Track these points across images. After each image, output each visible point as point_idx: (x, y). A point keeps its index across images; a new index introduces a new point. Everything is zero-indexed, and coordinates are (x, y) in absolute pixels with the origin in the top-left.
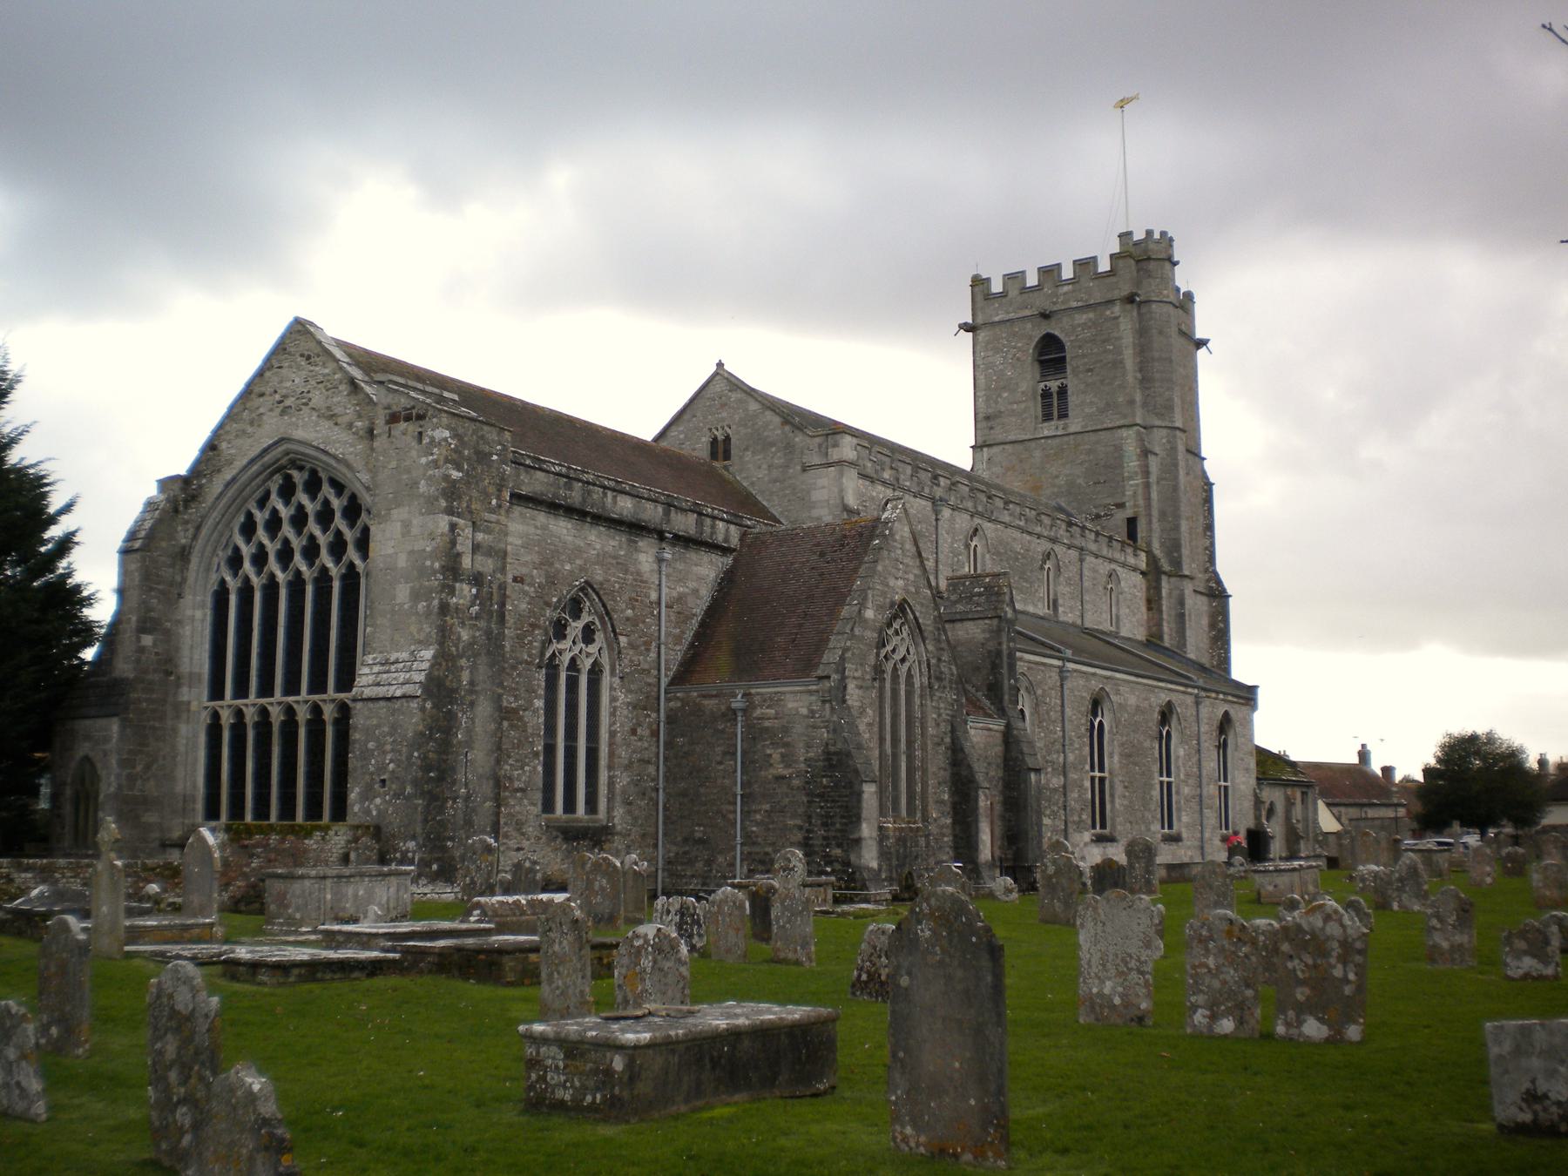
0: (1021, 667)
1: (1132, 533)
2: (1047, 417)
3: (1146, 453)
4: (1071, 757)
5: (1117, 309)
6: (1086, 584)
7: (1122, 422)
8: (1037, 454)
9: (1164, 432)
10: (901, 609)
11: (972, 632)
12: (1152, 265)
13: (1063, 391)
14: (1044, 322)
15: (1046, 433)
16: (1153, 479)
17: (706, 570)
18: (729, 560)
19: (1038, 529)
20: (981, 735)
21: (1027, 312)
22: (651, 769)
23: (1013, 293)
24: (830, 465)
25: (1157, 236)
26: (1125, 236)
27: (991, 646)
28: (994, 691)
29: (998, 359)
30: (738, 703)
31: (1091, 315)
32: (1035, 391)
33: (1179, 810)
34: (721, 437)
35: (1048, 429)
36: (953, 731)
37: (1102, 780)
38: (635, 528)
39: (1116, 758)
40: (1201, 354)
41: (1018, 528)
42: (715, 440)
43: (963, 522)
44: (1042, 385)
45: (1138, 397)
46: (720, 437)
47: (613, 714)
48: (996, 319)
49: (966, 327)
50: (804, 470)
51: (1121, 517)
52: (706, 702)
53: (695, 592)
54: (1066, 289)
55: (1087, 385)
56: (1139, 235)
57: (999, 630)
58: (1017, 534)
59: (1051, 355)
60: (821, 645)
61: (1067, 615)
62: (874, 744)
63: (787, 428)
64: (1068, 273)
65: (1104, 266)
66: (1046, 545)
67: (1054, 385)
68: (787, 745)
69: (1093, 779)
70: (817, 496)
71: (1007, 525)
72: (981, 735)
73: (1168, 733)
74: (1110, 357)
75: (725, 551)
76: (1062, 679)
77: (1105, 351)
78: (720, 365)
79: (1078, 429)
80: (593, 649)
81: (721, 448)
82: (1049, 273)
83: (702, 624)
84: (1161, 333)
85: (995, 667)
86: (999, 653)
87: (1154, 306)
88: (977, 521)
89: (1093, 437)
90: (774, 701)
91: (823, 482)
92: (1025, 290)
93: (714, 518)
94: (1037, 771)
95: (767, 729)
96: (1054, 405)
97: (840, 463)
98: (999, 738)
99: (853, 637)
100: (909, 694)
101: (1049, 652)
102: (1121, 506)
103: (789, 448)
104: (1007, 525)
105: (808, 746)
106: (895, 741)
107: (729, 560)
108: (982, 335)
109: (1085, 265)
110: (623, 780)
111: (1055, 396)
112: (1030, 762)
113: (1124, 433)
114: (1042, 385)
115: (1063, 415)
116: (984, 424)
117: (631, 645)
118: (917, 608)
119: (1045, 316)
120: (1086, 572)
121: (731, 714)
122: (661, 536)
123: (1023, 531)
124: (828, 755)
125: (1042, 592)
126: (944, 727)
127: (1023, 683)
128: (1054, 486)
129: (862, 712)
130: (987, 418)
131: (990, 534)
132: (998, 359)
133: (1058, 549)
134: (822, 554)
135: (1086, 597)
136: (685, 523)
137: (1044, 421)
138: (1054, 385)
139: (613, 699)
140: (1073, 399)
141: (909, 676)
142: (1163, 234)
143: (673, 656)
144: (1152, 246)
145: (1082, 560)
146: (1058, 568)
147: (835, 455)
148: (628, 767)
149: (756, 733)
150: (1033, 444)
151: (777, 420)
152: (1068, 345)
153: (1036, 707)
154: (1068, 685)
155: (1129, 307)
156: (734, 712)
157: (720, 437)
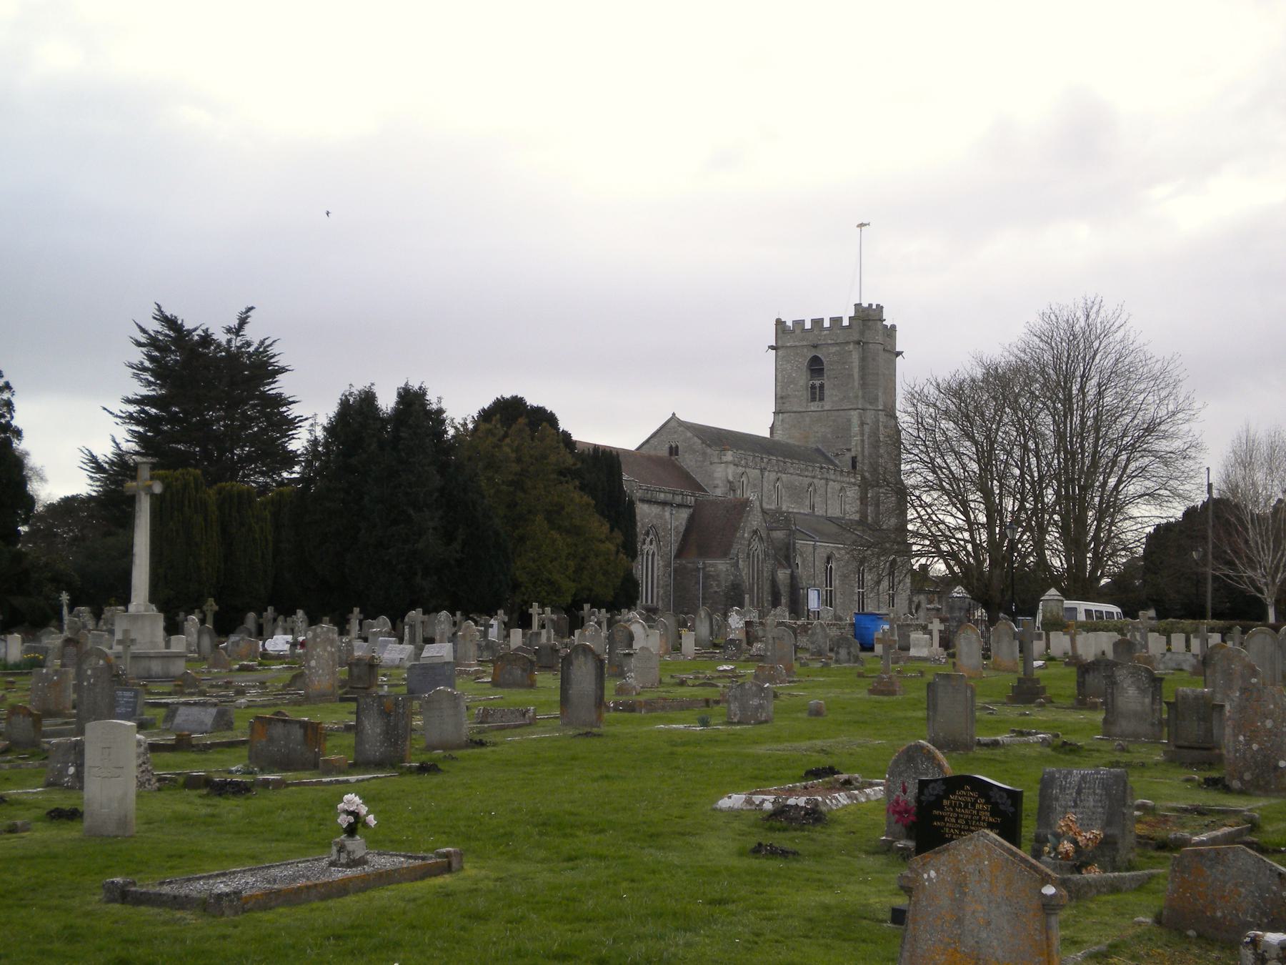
0: (798, 546)
1: (854, 466)
2: (813, 399)
3: (862, 424)
4: (817, 582)
5: (851, 346)
6: (829, 495)
7: (851, 407)
8: (808, 419)
9: (873, 412)
10: (755, 532)
11: (779, 535)
12: (870, 323)
13: (822, 386)
14: (813, 350)
15: (812, 409)
16: (866, 437)
17: (684, 514)
18: (692, 510)
19: (806, 473)
20: (783, 575)
21: (805, 343)
22: (669, 588)
23: (798, 331)
24: (722, 463)
25: (874, 307)
26: (858, 306)
27: (786, 541)
28: (787, 558)
29: (789, 367)
30: (701, 566)
31: (838, 348)
32: (807, 386)
33: (867, 604)
34: (674, 446)
35: (814, 406)
36: (773, 575)
37: (831, 591)
38: (664, 504)
39: (837, 582)
40: (899, 359)
41: (797, 474)
42: (671, 446)
43: (773, 476)
44: (811, 382)
45: (860, 394)
46: (154, 326)
47: (658, 569)
48: (788, 344)
49: (771, 347)
50: (711, 464)
51: (848, 456)
52: (689, 565)
53: (681, 523)
54: (825, 332)
55: (834, 385)
56: (865, 305)
57: (789, 535)
58: (797, 477)
59: (816, 367)
60: (730, 546)
61: (819, 511)
62: (747, 581)
63: (704, 445)
64: (827, 324)
65: (846, 323)
66: (809, 480)
67: (817, 383)
68: (718, 581)
69: (827, 591)
70: (716, 475)
71: (792, 474)
72: (783, 575)
73: (863, 570)
74: (847, 372)
75: (690, 507)
76: (815, 549)
77: (845, 369)
78: (674, 414)
79: (829, 408)
80: (652, 547)
81: (674, 451)
82: (817, 323)
83: (684, 535)
84: (874, 360)
85: (788, 549)
86: (789, 544)
87: (871, 345)
88: (779, 474)
89: (836, 413)
90: (713, 565)
91: (719, 469)
92: (804, 330)
93: (687, 495)
94: (803, 589)
95: (711, 575)
96: (816, 394)
97: (726, 462)
98: (788, 576)
99: (741, 544)
100: (758, 562)
101: (810, 538)
102: (849, 450)
103: (704, 454)
104: (792, 474)
105: (726, 581)
106: (753, 579)
107: (692, 510)
108: (780, 353)
109: (836, 321)
110: (661, 592)
111: (818, 390)
112: (801, 586)
113: (852, 413)
114: (811, 382)
115: (822, 399)
116: (780, 401)
117: (664, 545)
118: (761, 531)
119: (815, 347)
120: (829, 490)
121: (698, 569)
122: (672, 505)
123: (799, 475)
124: (733, 585)
125: (807, 503)
126: (770, 573)
127: (798, 552)
128: (815, 437)
129: (743, 569)
130: (782, 398)
131: (784, 479)
132: (789, 367)
133: (816, 481)
134: (728, 511)
135: (829, 502)
136: (678, 499)
137: (812, 401)
138: (817, 383)
139: (658, 564)
140: (827, 392)
141: (758, 555)
142: (878, 305)
143: (674, 548)
144: (871, 313)
145: (827, 485)
146: (815, 490)
147: (725, 459)
148: (663, 587)
149: (707, 577)
150: (805, 414)
151: (700, 441)
152: (825, 363)
153: (803, 562)
154: (817, 551)
155: (857, 346)
156: (699, 569)
157: (154, 326)
